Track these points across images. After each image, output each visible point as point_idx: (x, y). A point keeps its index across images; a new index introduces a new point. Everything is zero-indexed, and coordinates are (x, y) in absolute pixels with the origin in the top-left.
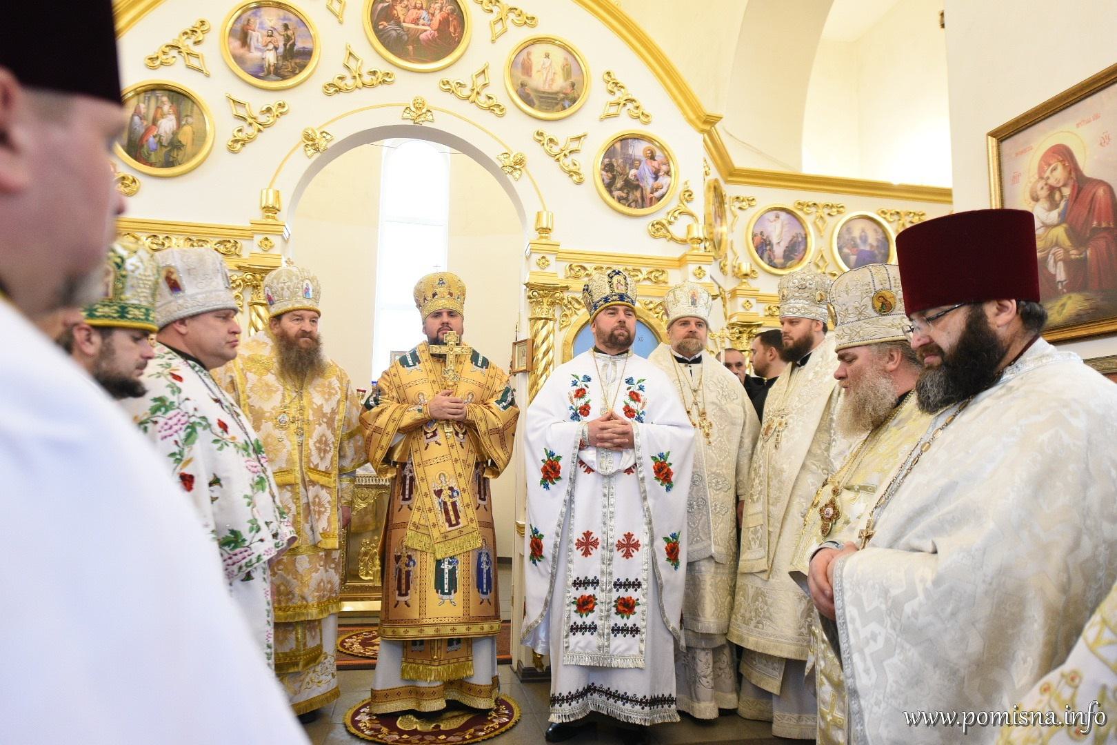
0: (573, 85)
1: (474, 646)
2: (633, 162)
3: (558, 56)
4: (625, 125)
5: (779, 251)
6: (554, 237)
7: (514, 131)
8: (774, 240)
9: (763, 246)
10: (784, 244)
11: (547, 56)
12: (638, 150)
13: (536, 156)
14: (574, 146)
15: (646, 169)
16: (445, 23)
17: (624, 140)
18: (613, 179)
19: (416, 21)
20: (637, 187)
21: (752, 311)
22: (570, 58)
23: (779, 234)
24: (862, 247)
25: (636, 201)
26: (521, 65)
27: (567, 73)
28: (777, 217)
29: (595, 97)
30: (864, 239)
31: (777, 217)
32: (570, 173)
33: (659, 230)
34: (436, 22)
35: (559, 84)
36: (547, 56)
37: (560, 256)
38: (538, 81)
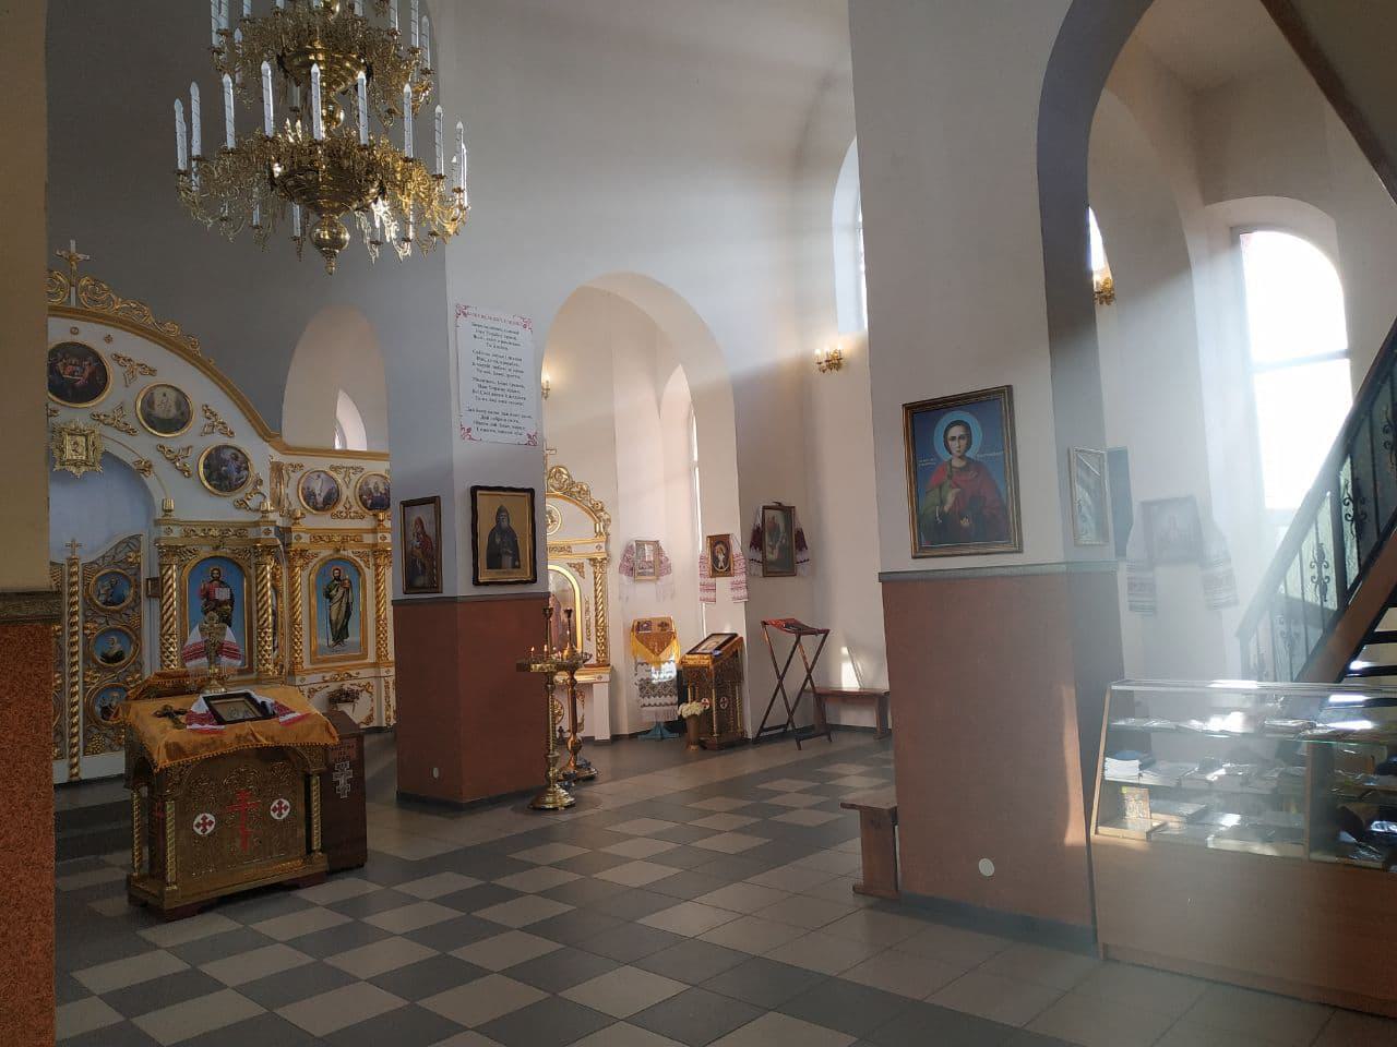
0: (182, 414)
1: (1243, 237)
2: (224, 462)
3: (172, 395)
4: (219, 440)
5: (320, 499)
6: (174, 515)
7: (142, 446)
8: (317, 492)
9: (309, 496)
10: (323, 494)
11: (165, 395)
12: (227, 455)
13: (161, 466)
14: (184, 454)
15: (233, 466)
16: (92, 374)
17: (218, 449)
18: (210, 474)
19: (72, 374)
20: (226, 478)
21: (302, 540)
22: (180, 398)
23: (319, 488)
24: (375, 495)
25: (226, 486)
26: (149, 402)
27: (178, 405)
28: (319, 476)
29: (198, 420)
30: (377, 489)
31: (319, 476)
32: (183, 471)
33: (242, 505)
34: (86, 374)
35: (173, 412)
36: (165, 395)
37: (178, 523)
38: (159, 411)
